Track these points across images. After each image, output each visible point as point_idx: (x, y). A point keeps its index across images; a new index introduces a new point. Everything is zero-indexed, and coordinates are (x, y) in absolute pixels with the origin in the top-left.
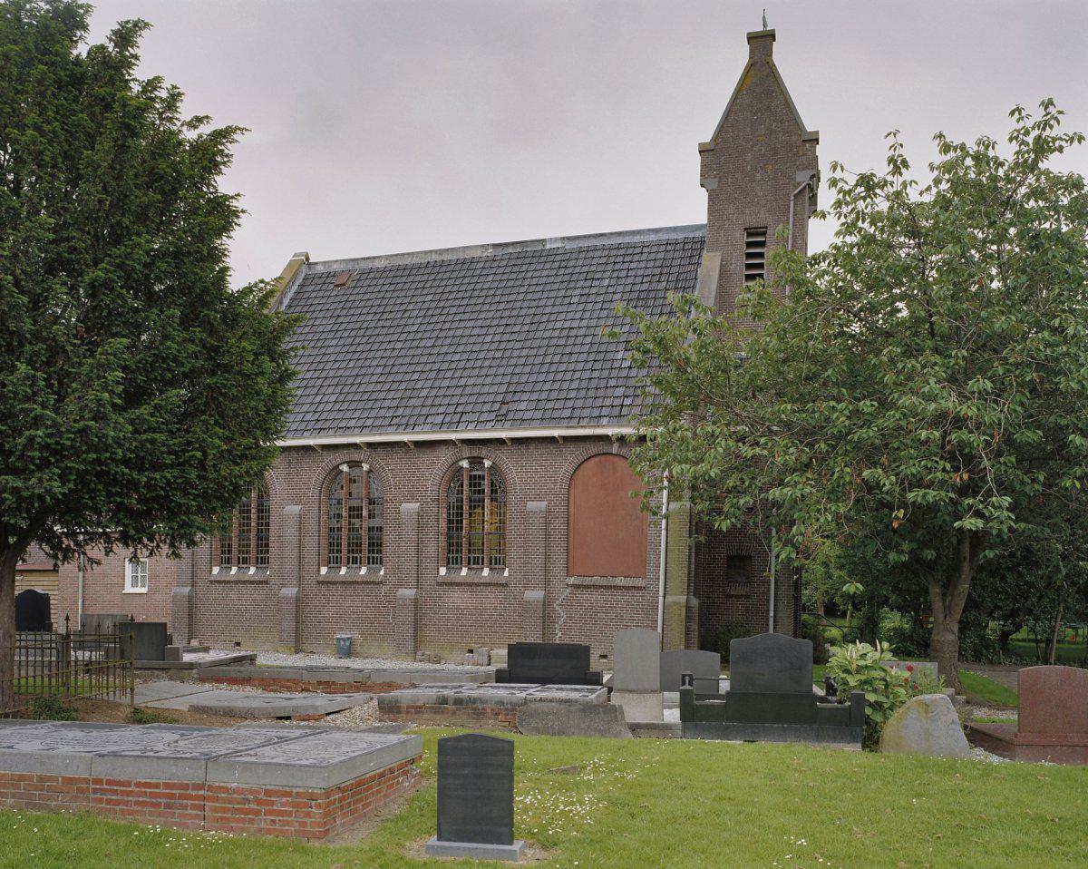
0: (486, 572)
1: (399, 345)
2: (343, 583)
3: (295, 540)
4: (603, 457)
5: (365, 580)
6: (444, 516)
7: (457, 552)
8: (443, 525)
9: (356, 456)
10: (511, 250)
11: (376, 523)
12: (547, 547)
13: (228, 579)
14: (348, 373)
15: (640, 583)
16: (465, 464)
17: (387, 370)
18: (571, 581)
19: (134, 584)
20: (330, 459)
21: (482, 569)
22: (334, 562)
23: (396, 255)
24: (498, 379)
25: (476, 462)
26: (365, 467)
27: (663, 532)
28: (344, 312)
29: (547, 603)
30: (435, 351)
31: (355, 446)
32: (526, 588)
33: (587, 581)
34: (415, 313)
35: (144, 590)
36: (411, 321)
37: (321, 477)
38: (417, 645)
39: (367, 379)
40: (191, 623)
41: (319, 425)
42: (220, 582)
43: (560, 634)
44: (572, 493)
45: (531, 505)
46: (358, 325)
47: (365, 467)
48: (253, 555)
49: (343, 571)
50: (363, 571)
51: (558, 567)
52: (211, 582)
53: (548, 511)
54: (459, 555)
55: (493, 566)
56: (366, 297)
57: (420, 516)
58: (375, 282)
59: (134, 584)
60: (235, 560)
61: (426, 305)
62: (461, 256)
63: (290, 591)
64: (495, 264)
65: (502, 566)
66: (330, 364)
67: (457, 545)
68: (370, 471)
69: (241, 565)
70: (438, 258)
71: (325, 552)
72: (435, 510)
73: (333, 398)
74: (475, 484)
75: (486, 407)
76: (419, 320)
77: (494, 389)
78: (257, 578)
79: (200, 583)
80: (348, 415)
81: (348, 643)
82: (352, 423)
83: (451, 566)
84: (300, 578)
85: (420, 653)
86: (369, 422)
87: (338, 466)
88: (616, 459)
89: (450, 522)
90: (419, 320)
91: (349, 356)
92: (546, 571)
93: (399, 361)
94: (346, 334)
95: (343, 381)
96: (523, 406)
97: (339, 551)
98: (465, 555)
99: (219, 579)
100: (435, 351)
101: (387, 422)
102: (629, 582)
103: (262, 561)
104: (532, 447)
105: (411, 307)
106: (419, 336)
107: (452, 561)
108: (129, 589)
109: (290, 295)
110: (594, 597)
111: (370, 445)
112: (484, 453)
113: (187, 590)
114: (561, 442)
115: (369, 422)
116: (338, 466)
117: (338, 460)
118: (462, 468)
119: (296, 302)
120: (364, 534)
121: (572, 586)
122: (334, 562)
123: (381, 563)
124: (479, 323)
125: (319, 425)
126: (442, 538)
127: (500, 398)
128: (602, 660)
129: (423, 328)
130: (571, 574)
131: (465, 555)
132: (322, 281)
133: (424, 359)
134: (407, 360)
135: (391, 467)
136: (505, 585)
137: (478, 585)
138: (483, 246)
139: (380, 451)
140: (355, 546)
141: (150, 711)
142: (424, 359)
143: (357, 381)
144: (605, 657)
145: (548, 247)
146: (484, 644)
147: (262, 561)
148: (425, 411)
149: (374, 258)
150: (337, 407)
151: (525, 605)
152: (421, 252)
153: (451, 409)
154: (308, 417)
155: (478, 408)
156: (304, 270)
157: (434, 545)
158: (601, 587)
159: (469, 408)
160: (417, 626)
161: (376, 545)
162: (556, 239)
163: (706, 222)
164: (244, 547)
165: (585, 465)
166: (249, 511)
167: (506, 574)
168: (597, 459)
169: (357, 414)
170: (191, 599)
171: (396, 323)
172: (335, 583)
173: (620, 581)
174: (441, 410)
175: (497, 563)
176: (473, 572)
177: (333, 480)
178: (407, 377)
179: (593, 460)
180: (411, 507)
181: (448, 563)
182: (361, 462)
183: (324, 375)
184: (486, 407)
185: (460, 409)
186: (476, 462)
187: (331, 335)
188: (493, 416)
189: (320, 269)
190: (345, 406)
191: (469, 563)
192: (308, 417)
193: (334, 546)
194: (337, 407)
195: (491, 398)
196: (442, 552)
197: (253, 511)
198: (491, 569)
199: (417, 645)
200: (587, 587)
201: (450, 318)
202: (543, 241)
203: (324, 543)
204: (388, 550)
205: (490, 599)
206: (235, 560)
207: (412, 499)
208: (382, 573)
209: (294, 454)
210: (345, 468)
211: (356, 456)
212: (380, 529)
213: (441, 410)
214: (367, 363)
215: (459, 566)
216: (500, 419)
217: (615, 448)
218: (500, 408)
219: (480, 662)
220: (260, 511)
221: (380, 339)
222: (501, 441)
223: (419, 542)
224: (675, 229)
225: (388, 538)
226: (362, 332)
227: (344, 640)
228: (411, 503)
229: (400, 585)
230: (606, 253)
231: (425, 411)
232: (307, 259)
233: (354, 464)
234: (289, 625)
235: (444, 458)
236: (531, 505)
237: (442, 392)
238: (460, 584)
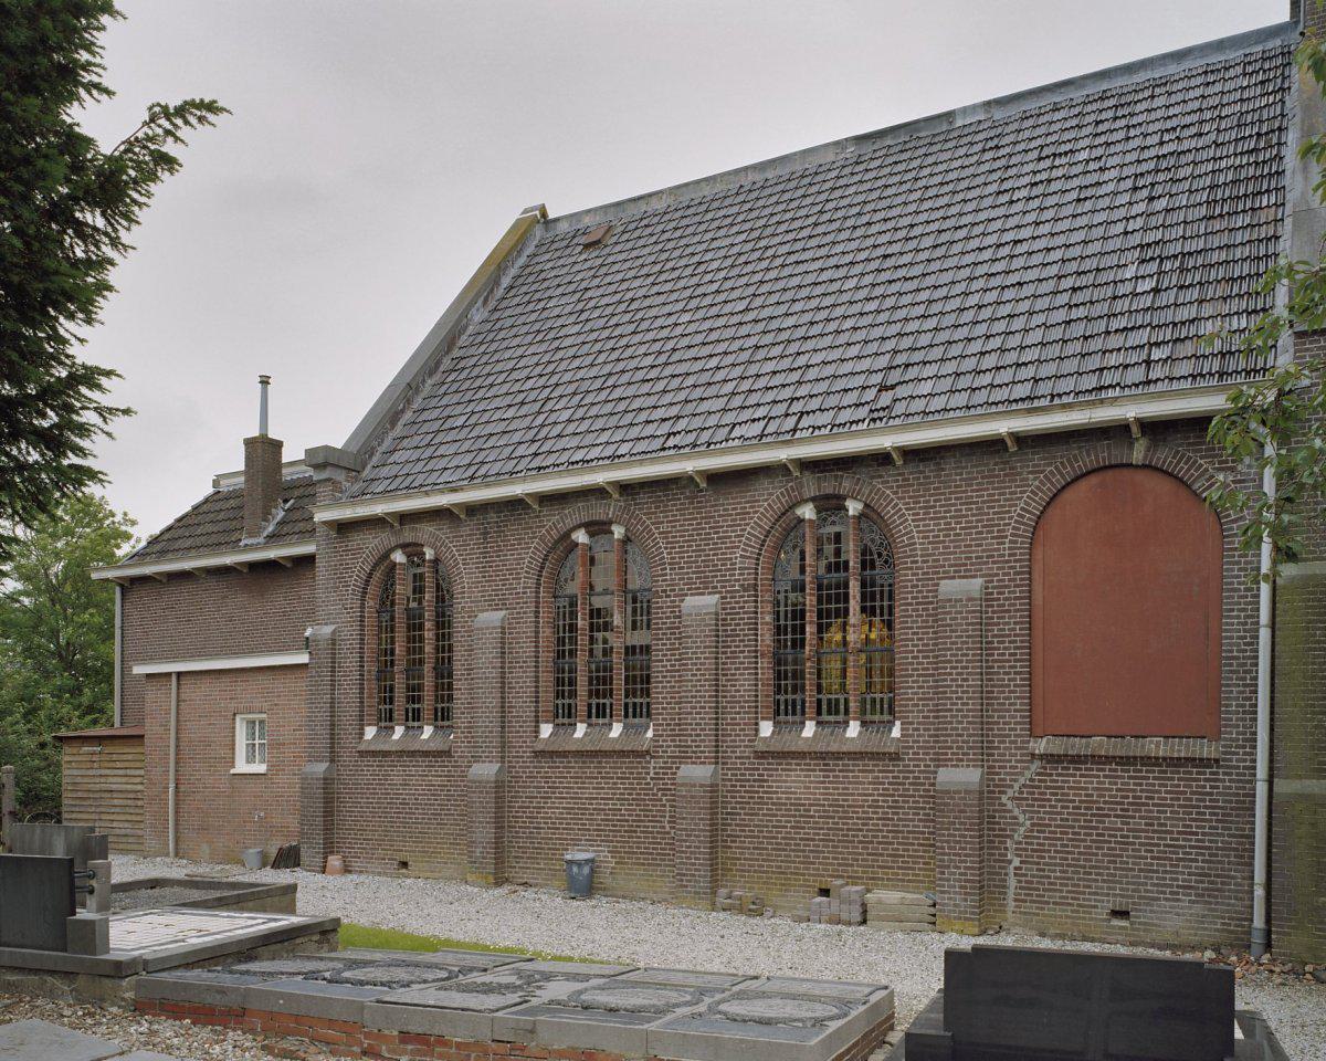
0: (854, 729)
1: (686, 317)
2: (579, 754)
3: (495, 673)
4: (1110, 474)
5: (617, 748)
6: (768, 618)
7: (795, 691)
8: (766, 638)
9: (599, 511)
10: (889, 142)
11: (638, 638)
12: (987, 674)
13: (386, 748)
14: (593, 372)
15: (1206, 750)
16: (807, 512)
17: (662, 359)
18: (1041, 746)
19: (250, 760)
20: (553, 522)
21: (847, 723)
22: (386, 720)
23: (686, 185)
24: (873, 348)
25: (830, 505)
26: (618, 532)
28: (596, 282)
29: (989, 793)
30: (751, 316)
31: (598, 492)
32: (940, 761)
33: (1077, 746)
34: (715, 265)
35: (262, 768)
36: (708, 277)
37: (539, 557)
38: (717, 873)
39: (625, 378)
40: (328, 828)
41: (537, 462)
42: (374, 753)
43: (1016, 862)
44: (1039, 554)
45: (948, 587)
46: (618, 297)
47: (618, 532)
49: (581, 730)
50: (617, 730)
51: (1011, 717)
52: (362, 754)
53: (987, 598)
54: (798, 697)
55: (869, 717)
56: (635, 253)
57: (720, 620)
58: (649, 230)
59: (250, 760)
60: (427, 714)
61: (736, 250)
62: (798, 168)
63: (486, 770)
64: (861, 167)
65: (886, 717)
66: (565, 363)
67: (795, 677)
68: (626, 540)
69: (410, 723)
70: (759, 177)
71: (548, 694)
72: (750, 607)
73: (566, 415)
75: (851, 398)
76: (722, 274)
77: (865, 364)
78: (433, 746)
79: (346, 757)
80: (589, 439)
81: (586, 870)
82: (595, 453)
83: (782, 718)
84: (503, 745)
85: (723, 891)
86: (624, 449)
87: (567, 535)
89: (779, 630)
90: (722, 274)
91: (598, 346)
92: (985, 726)
93: (685, 342)
94: (596, 313)
95: (585, 386)
97: (573, 694)
98: (810, 695)
99: (372, 748)
100: (751, 316)
101: (657, 444)
102: (1180, 749)
103: (442, 716)
104: (949, 465)
105: (709, 256)
106: (722, 297)
107: (786, 710)
108: (242, 767)
109: (513, 272)
110: (1093, 782)
111: (626, 488)
112: (846, 485)
113: (321, 768)
114: (1013, 448)
115: (624, 449)
116: (567, 535)
117: (569, 523)
118: (801, 521)
119: (521, 281)
120: (617, 660)
121: (1042, 757)
122: (565, 716)
123: (891, 711)
124: (833, 261)
125: (537, 462)
126: (765, 664)
127: (877, 379)
128: (1116, 922)
129: (729, 284)
130: (1039, 731)
131: (810, 695)
132: (565, 243)
133: (729, 333)
134: (699, 339)
135: (667, 528)
136: (895, 757)
137: (838, 756)
138: (837, 143)
139: (643, 498)
140: (601, 683)
142: (729, 333)
143: (609, 383)
144: (1123, 914)
145: (959, 123)
146: (854, 880)
147: (442, 716)
148: (729, 418)
149: (650, 195)
150: (571, 428)
151: (937, 800)
152: (729, 173)
153: (780, 409)
154: (521, 451)
155: (833, 401)
156: (539, 232)
157: (750, 677)
158: (1109, 759)
159: (814, 404)
160: (717, 838)
161: (640, 682)
162: (974, 108)
163: (1288, 19)
164: (414, 695)
165: (1068, 495)
166: (421, 627)
167: (896, 732)
168: (1094, 480)
169: (604, 437)
170: (327, 781)
171: (682, 283)
172: (564, 754)
173: (1155, 747)
174: (760, 412)
175: (638, 711)
176: (827, 730)
177: (562, 561)
178: (698, 365)
179: (1083, 485)
181: (777, 713)
182: (611, 523)
183: (553, 380)
184: (851, 398)
185: (797, 407)
186: (830, 505)
187: (572, 319)
188: (862, 412)
189: (563, 227)
190: (584, 427)
191: (819, 713)
192: (521, 451)
193: (564, 684)
194: (571, 428)
195: (859, 381)
196: (766, 691)
197: (428, 625)
198: (864, 724)
199: (717, 873)
200: (1077, 760)
201: (778, 262)
202: (949, 116)
203: (547, 679)
204: (661, 691)
205: (863, 784)
206: (427, 714)
207: (705, 587)
208: (650, 734)
209: (493, 517)
210: (581, 537)
211: (599, 511)
212: (646, 649)
213: (760, 412)
214: (629, 352)
215: (797, 718)
216: (879, 417)
217: (1138, 453)
218: (877, 398)
219: (844, 916)
221: (653, 312)
222: (881, 459)
223: (719, 671)
224: (1220, 45)
225: (660, 666)
226: (623, 307)
227: (579, 864)
228: (705, 600)
229: (684, 757)
230: (1076, 110)
231: (729, 418)
232: (544, 215)
233: (598, 528)
234: (484, 833)
235: (766, 500)
236: (948, 587)
237: (761, 383)
238: (801, 755)
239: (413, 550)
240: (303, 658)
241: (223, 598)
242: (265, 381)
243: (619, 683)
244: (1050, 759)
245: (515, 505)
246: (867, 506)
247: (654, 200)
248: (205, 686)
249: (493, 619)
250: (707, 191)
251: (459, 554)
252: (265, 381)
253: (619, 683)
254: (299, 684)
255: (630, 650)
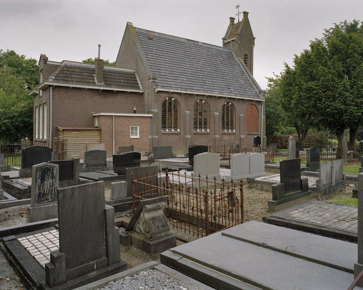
18: (247, 133)
22: (228, 128)
27: (262, 121)
48: (173, 125)
54: (201, 126)
65: (176, 129)
74: (170, 105)
88: (254, 106)
96: (86, 74)
99: (205, 133)
135: (212, 102)
140: (201, 124)
141: (107, 189)
147: (232, 129)
161: (205, 123)
180: (217, 113)
193: (195, 123)
202: (198, 42)
205: (233, 137)
220: (165, 109)
222: (235, 99)
235: (223, 100)
239: (170, 98)
240: (152, 115)
241: (92, 96)
242: (99, 46)
243: (203, 124)
244: (248, 134)
245: (192, 95)
246: (169, 97)
247: (155, 33)
248: (122, 119)
249: (186, 112)
250: (164, 36)
251: (180, 99)
252: (99, 46)
253: (203, 124)
254: (149, 120)
255: (204, 119)
